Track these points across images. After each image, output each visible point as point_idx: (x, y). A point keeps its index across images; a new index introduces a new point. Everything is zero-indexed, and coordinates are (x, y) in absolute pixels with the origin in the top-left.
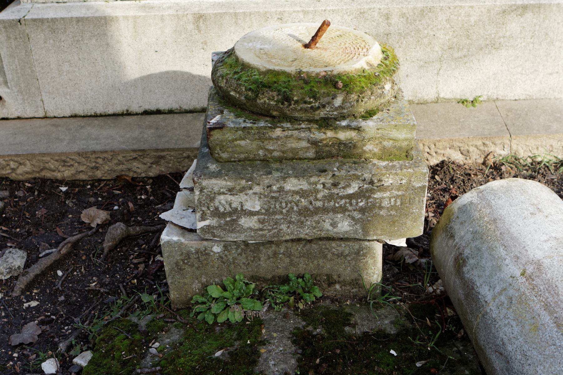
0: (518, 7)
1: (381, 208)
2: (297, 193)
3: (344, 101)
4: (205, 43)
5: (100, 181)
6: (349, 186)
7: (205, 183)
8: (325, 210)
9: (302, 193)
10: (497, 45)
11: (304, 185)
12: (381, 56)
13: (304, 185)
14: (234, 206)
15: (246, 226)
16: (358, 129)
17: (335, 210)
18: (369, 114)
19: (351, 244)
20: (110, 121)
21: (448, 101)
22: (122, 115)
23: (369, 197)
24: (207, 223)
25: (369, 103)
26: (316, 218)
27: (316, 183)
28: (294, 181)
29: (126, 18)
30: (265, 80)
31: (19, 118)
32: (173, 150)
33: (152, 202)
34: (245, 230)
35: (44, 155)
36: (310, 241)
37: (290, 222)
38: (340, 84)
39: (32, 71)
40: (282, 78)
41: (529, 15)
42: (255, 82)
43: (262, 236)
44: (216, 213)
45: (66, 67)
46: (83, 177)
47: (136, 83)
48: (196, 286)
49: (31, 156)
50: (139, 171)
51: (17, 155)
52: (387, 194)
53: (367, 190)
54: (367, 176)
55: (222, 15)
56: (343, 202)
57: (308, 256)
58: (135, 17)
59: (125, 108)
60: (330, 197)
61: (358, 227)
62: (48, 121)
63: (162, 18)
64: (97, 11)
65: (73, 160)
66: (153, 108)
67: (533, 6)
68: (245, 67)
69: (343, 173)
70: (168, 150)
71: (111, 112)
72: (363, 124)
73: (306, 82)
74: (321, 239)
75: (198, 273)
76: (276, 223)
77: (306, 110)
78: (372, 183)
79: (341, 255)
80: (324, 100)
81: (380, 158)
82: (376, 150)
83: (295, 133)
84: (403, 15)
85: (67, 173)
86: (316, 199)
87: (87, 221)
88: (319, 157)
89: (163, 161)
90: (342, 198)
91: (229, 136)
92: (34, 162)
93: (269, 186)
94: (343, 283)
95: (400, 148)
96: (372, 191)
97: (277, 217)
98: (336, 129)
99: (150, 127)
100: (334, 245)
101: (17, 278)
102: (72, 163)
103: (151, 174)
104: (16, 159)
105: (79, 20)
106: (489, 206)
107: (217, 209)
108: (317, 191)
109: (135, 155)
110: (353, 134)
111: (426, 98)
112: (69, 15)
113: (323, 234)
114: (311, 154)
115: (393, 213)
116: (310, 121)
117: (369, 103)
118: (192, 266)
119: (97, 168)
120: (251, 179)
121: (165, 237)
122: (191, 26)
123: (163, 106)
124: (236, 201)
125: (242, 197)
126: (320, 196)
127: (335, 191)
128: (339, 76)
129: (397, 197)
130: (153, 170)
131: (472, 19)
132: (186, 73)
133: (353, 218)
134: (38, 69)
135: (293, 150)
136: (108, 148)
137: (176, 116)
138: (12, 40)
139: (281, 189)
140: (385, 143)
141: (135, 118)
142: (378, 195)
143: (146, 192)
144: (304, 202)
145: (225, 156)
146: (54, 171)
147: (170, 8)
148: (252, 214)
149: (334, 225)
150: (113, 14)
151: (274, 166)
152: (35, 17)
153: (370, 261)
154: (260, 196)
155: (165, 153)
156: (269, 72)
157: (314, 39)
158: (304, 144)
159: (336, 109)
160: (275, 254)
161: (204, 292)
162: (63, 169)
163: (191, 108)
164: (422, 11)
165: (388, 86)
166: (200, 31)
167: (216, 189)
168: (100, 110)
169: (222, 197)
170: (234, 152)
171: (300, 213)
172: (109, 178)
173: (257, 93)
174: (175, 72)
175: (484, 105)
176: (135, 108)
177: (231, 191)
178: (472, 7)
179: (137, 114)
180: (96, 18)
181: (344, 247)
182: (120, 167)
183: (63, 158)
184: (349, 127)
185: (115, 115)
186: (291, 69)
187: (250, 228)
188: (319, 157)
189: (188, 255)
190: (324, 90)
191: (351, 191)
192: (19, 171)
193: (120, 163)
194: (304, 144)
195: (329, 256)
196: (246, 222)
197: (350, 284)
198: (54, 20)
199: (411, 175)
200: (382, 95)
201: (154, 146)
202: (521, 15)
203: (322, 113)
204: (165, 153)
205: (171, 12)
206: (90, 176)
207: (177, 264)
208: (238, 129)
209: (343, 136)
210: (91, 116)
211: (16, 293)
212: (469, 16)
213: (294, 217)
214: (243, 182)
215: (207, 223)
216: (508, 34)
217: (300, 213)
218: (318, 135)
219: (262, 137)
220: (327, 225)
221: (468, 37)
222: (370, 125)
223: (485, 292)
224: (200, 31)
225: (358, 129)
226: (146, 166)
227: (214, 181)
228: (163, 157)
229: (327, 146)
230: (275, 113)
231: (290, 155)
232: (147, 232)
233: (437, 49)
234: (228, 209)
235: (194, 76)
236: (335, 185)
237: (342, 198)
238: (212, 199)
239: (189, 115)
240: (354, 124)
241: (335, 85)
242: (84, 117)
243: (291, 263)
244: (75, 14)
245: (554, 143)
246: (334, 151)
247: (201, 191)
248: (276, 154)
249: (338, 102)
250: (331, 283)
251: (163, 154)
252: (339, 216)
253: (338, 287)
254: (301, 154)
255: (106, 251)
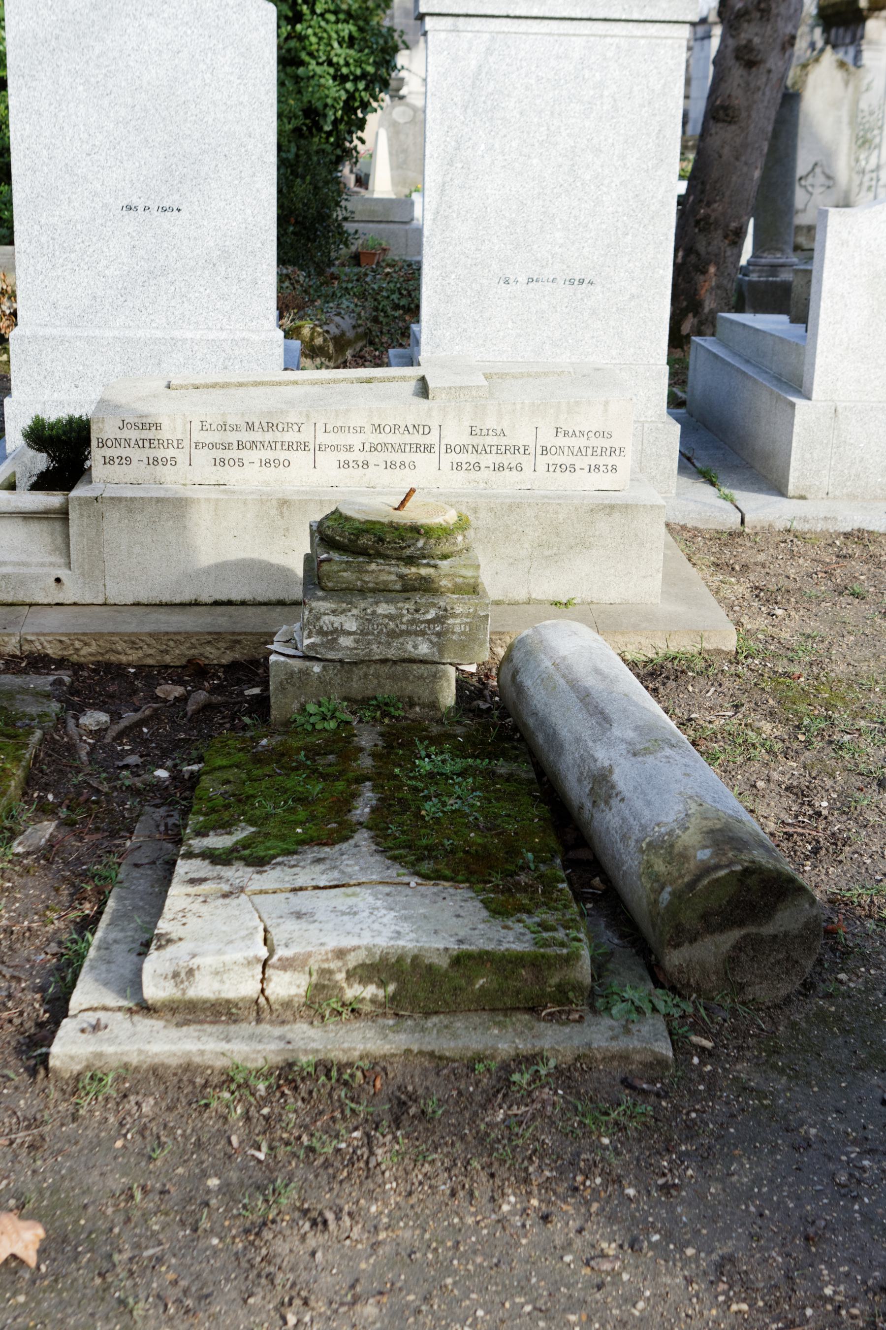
0: (605, 507)
1: (453, 633)
2: (386, 616)
3: (425, 544)
4: (287, 530)
5: (167, 667)
6: (428, 612)
7: (314, 604)
8: (408, 633)
9: (391, 617)
10: (587, 545)
11: (391, 609)
12: (456, 519)
13: (391, 609)
14: (335, 625)
15: (344, 644)
16: (435, 566)
17: (416, 634)
18: (445, 557)
19: (429, 666)
20: (177, 609)
21: (540, 602)
22: (190, 604)
23: (444, 623)
24: (312, 640)
25: (445, 548)
26: (401, 640)
27: (401, 609)
28: (384, 605)
29: (208, 500)
30: (364, 527)
31: (75, 604)
32: (251, 634)
33: (226, 686)
34: (343, 649)
35: (112, 634)
36: (395, 662)
37: (379, 643)
38: (422, 531)
39: (100, 552)
40: (378, 526)
41: (617, 515)
42: (356, 529)
43: (357, 654)
44: (321, 632)
45: (137, 549)
46: (150, 661)
47: (208, 571)
48: (296, 706)
49: (97, 636)
50: (211, 656)
51: (84, 634)
52: (458, 621)
53: (442, 616)
54: (442, 604)
55: (307, 502)
56: (423, 626)
57: (393, 677)
58: (217, 500)
59: (193, 597)
60: (413, 622)
61: (435, 649)
62: (108, 608)
63: (245, 503)
64: (176, 493)
65: (143, 641)
66: (224, 597)
67: (621, 506)
68: (348, 519)
69: (423, 600)
70: (245, 633)
71: (178, 601)
72: (439, 562)
73: (397, 529)
74: (404, 661)
75: (298, 692)
76: (368, 644)
77: (396, 549)
78: (446, 610)
79: (421, 677)
80: (409, 542)
81: (453, 593)
82: (450, 585)
83: (387, 568)
84: (491, 510)
85: (133, 656)
86: (402, 623)
87: (162, 696)
88: (404, 590)
89: (238, 646)
90: (422, 622)
91: (335, 568)
92: (101, 643)
93: (365, 610)
94: (423, 706)
95: (468, 585)
96: (446, 617)
97: (370, 637)
98: (418, 565)
99: (223, 615)
100: (415, 667)
101: (106, 730)
102: (141, 644)
103: (224, 661)
104: (82, 638)
105: (158, 500)
106: (540, 634)
107: (321, 627)
108: (402, 616)
109: (209, 638)
110: (431, 571)
111: (517, 598)
112: (149, 495)
113: (406, 656)
114: (398, 587)
115: (463, 638)
116: (399, 559)
117: (445, 548)
118: (294, 685)
119: (166, 652)
120: (350, 603)
121: (273, 658)
122: (274, 512)
123: (235, 596)
124: (337, 621)
125: (342, 618)
126: (405, 620)
127: (417, 616)
128: (422, 526)
129: (466, 623)
130: (226, 657)
131: (561, 517)
132: (264, 561)
133: (431, 642)
134: (106, 550)
135: (384, 582)
136: (181, 630)
137: (249, 608)
138: (85, 519)
139: (374, 613)
140: (457, 580)
141: (204, 608)
142: (451, 621)
143: (219, 678)
144: (392, 625)
145: (330, 584)
146: (119, 653)
147: (252, 493)
148: (349, 633)
149: (415, 647)
150: (195, 496)
151: (369, 595)
152: (113, 495)
153: (445, 684)
154: (357, 617)
155: (241, 637)
156: (367, 521)
157: (403, 503)
158: (393, 577)
159: (419, 549)
160: (366, 675)
161: (303, 709)
162: (130, 652)
163: (266, 600)
164: (510, 506)
165: (460, 538)
166: (282, 517)
167: (322, 610)
168: (166, 598)
169: (326, 617)
170: (337, 582)
171: (388, 635)
172: (178, 664)
173: (357, 536)
174: (252, 560)
175: (578, 607)
176: (205, 598)
177: (334, 612)
178: (559, 504)
179: (206, 604)
180: (177, 499)
181: (423, 669)
182: (193, 651)
183: (133, 639)
184: (428, 565)
185: (182, 605)
186: (386, 520)
187: (347, 647)
188: (404, 590)
189: (291, 674)
190: (409, 535)
191: (429, 617)
192: (83, 652)
193: (193, 647)
194: (393, 577)
195: (411, 678)
196: (345, 641)
197: (428, 706)
198: (132, 500)
199: (477, 605)
200: (454, 544)
201: (231, 630)
202: (609, 515)
203: (408, 552)
204: (241, 637)
205: (254, 496)
206: (158, 661)
207: (281, 683)
208: (342, 563)
209: (424, 571)
210: (155, 605)
211: (108, 740)
212: (557, 513)
213: (384, 639)
214: (344, 605)
215: (312, 640)
216: (597, 533)
217: (388, 635)
218: (405, 570)
219: (361, 571)
220: (409, 647)
221: (557, 534)
222: (444, 564)
223: (528, 683)
224: (282, 517)
225: (435, 566)
226: (220, 652)
227: (321, 603)
228: (238, 642)
229: (411, 579)
230: (371, 552)
231: (382, 587)
232: (227, 702)
233: (526, 546)
234: (331, 628)
235: (272, 565)
236: (417, 611)
237: (422, 622)
238: (318, 619)
239: (264, 608)
240: (432, 562)
241: (418, 532)
242: (147, 605)
243: (379, 685)
244: (155, 494)
245: (643, 641)
246: (417, 585)
247: (310, 611)
248: (371, 585)
249: (420, 544)
250: (412, 705)
251: (239, 638)
252: (420, 638)
253: (417, 709)
254: (391, 587)
255: (189, 714)
